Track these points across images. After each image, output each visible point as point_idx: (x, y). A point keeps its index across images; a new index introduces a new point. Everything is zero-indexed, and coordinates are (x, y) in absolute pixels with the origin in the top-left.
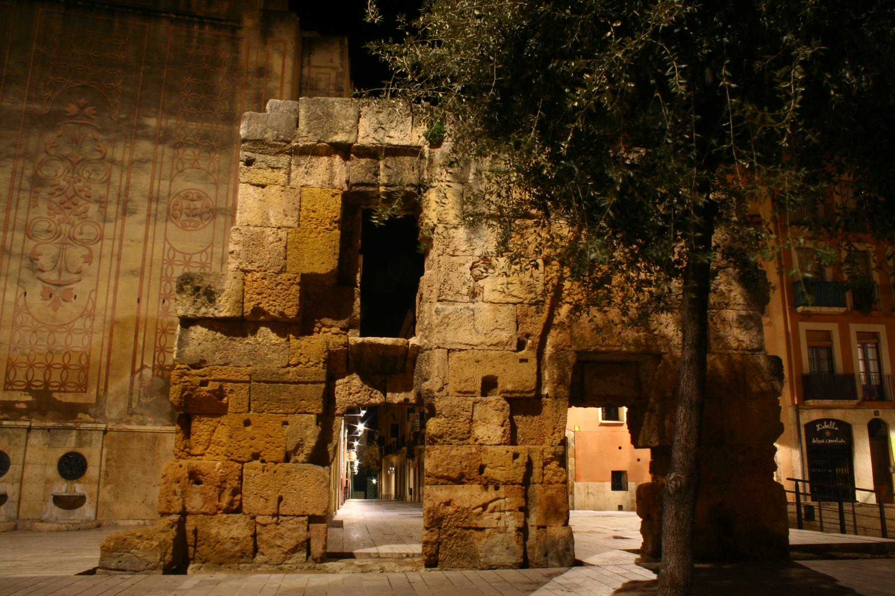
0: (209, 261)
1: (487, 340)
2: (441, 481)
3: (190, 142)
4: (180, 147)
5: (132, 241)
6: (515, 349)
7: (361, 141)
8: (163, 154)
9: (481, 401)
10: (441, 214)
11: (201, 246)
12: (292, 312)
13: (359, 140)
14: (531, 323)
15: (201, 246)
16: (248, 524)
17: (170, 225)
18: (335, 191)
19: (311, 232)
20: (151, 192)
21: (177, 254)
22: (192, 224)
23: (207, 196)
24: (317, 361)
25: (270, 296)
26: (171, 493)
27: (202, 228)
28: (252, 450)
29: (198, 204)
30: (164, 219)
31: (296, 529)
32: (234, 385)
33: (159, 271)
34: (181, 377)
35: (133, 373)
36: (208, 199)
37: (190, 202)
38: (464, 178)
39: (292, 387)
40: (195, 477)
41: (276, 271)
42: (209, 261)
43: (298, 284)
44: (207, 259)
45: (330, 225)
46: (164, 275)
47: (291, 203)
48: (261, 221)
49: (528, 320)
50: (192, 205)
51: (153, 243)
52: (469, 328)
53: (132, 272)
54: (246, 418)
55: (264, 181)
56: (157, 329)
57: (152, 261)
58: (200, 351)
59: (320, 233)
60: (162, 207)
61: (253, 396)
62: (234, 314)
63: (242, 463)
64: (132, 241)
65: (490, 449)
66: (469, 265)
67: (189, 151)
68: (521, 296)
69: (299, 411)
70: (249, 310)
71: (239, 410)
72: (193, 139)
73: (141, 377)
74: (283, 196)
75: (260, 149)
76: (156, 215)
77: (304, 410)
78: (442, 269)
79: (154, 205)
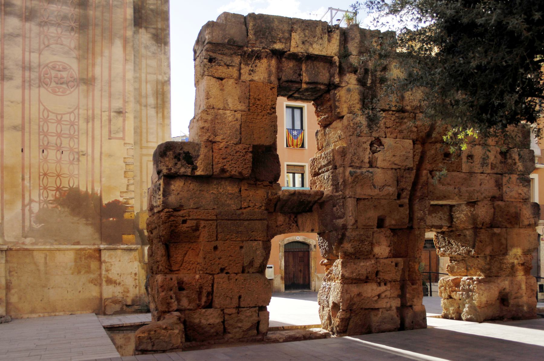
0: (76, 120)
1: (381, 193)
2: (354, 282)
3: (53, 22)
4: (44, 26)
5: (12, 102)
6: (396, 198)
7: (293, 50)
8: (30, 30)
9: (377, 231)
10: (351, 107)
11: (69, 108)
12: (247, 172)
13: (291, 50)
14: (405, 182)
15: (69, 108)
16: (219, 315)
17: (42, 90)
18: (272, 85)
19: (258, 115)
20: (24, 62)
21: (50, 114)
22: (61, 90)
23: (71, 68)
24: (261, 205)
25: (232, 160)
26: (169, 298)
27: (68, 94)
28: (220, 266)
29: (65, 74)
30: (37, 85)
31: (251, 316)
32: (205, 222)
33: (37, 127)
34: (169, 218)
35: (24, 206)
36: (72, 70)
37: (58, 72)
38: (365, 82)
39: (246, 223)
40: (181, 286)
41: (235, 143)
42: (76, 120)
43: (251, 152)
44: (75, 119)
45: (270, 110)
46: (41, 130)
47: (244, 93)
48: (223, 105)
49: (404, 180)
50: (59, 74)
51: (30, 105)
52: (369, 185)
53: (15, 128)
54: (215, 245)
55: (223, 76)
56: (39, 172)
57: (30, 119)
58: (179, 199)
59: (264, 116)
60: (34, 75)
61: (220, 230)
62: (207, 173)
63: (213, 275)
64: (12, 102)
65: (382, 261)
66: (369, 142)
67: (53, 29)
68: (400, 164)
69: (251, 239)
70: (218, 170)
71: (210, 240)
72: (55, 19)
73: (30, 211)
74: (237, 88)
75: (220, 50)
76: (30, 81)
77: (254, 238)
78: (353, 145)
79: (27, 74)
